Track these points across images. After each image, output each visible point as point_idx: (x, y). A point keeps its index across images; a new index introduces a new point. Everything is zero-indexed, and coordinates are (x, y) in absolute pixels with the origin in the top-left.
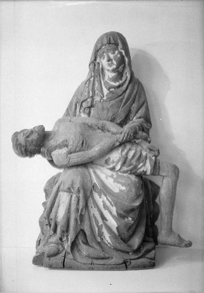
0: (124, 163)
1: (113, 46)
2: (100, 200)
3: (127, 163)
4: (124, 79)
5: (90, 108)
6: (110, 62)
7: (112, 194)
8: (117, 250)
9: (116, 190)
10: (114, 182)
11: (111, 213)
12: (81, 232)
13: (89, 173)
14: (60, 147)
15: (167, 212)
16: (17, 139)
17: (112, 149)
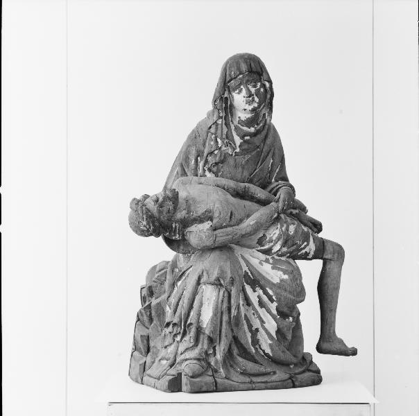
6: (251, 99)
10: (273, 268)
11: (269, 311)
14: (200, 220)
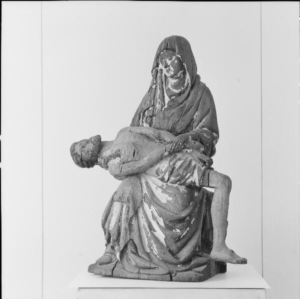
0: (171, 173)
1: (171, 52)
2: (149, 210)
3: (174, 173)
4: (186, 85)
5: (151, 117)
7: (159, 205)
8: (166, 262)
9: (164, 201)
10: (162, 192)
11: (158, 223)
12: (131, 241)
13: (141, 183)
15: (217, 225)
16: (74, 149)
17: (161, 159)
